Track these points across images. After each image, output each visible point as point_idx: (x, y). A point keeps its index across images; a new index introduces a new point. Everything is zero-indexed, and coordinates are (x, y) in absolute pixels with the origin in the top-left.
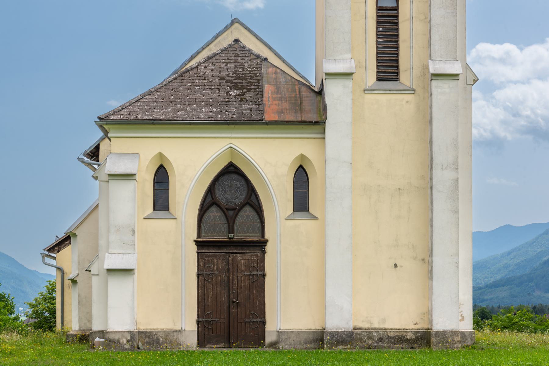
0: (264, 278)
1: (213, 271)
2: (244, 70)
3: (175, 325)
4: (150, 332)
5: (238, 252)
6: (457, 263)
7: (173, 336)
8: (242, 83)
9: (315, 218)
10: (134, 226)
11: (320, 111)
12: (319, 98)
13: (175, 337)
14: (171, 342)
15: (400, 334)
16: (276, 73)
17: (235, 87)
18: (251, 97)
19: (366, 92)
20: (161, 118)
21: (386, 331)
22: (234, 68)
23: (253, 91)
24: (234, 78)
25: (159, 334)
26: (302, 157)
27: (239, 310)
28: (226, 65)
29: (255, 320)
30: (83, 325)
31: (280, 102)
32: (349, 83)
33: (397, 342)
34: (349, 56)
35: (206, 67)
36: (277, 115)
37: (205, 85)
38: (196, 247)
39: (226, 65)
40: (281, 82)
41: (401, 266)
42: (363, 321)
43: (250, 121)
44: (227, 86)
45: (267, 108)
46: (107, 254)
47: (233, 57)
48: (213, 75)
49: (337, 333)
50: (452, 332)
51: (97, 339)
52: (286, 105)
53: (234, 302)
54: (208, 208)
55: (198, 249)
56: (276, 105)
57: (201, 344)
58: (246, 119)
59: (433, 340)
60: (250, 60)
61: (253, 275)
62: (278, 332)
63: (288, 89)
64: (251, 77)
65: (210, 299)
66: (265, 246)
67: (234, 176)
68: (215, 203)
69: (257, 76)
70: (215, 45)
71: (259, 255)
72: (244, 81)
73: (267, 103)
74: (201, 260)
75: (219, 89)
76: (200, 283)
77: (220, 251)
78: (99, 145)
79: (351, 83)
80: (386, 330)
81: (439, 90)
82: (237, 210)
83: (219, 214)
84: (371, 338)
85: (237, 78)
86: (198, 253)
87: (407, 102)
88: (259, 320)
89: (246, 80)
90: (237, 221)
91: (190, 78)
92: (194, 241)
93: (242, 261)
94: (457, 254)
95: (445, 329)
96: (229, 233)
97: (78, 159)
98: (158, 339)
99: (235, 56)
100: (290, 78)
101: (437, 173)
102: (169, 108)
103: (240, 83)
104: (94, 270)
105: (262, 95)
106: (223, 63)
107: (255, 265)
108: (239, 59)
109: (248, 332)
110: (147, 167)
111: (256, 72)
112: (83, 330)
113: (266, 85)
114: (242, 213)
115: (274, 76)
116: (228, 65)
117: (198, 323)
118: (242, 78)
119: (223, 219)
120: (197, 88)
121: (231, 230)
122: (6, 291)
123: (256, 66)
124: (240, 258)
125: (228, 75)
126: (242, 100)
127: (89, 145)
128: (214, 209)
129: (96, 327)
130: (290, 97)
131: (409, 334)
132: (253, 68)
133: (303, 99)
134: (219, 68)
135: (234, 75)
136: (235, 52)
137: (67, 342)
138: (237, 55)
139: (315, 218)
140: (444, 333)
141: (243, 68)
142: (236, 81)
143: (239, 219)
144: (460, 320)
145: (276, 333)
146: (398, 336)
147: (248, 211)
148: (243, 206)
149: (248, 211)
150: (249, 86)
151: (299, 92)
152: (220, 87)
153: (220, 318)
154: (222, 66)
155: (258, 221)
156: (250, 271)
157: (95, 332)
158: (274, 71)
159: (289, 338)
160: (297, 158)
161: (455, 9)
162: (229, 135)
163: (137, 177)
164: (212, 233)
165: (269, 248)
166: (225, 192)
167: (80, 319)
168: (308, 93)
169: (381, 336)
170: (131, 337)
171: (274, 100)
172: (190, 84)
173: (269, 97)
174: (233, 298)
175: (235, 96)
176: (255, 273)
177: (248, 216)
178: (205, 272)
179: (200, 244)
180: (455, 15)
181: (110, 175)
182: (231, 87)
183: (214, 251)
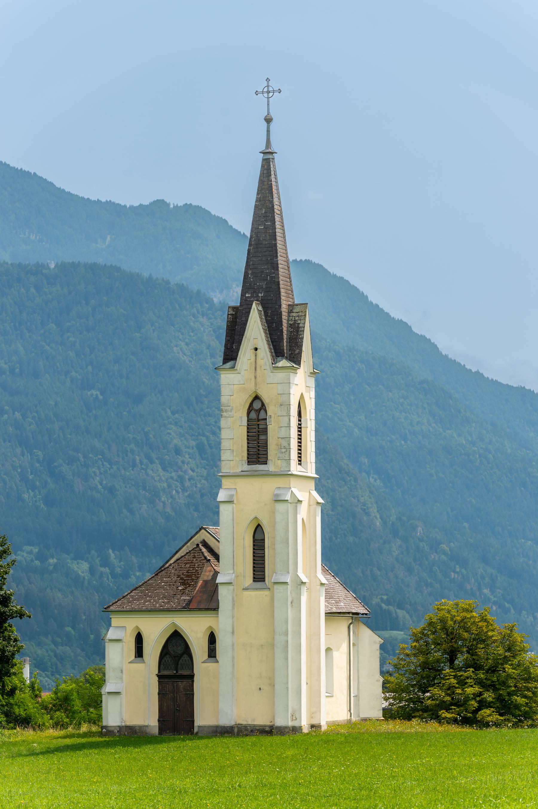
3: (145, 722)
4: (132, 726)
5: (179, 681)
6: (287, 688)
7: (144, 729)
10: (122, 667)
13: (145, 729)
14: (142, 732)
17: (183, 584)
19: (244, 590)
24: (186, 576)
25: (136, 727)
29: (189, 719)
32: (231, 587)
38: (157, 678)
41: (263, 689)
42: (243, 721)
49: (224, 727)
55: (159, 679)
57: (160, 733)
61: (187, 694)
62: (198, 726)
65: (165, 708)
71: (190, 682)
72: (190, 579)
80: (255, 726)
81: (278, 591)
84: (247, 730)
87: (266, 595)
90: (180, 663)
92: (156, 675)
93: (182, 686)
94: (287, 683)
95: (281, 725)
98: (136, 730)
107: (189, 688)
109: (185, 726)
110: (130, 634)
114: (182, 658)
117: (159, 721)
124: (180, 684)
131: (267, 728)
134: (181, 568)
140: (280, 727)
144: (295, 720)
147: (185, 657)
149: (185, 657)
155: (191, 663)
156: (186, 692)
162: (172, 616)
164: (167, 670)
169: (252, 729)
170: (119, 729)
172: (160, 581)
176: (188, 693)
179: (160, 677)
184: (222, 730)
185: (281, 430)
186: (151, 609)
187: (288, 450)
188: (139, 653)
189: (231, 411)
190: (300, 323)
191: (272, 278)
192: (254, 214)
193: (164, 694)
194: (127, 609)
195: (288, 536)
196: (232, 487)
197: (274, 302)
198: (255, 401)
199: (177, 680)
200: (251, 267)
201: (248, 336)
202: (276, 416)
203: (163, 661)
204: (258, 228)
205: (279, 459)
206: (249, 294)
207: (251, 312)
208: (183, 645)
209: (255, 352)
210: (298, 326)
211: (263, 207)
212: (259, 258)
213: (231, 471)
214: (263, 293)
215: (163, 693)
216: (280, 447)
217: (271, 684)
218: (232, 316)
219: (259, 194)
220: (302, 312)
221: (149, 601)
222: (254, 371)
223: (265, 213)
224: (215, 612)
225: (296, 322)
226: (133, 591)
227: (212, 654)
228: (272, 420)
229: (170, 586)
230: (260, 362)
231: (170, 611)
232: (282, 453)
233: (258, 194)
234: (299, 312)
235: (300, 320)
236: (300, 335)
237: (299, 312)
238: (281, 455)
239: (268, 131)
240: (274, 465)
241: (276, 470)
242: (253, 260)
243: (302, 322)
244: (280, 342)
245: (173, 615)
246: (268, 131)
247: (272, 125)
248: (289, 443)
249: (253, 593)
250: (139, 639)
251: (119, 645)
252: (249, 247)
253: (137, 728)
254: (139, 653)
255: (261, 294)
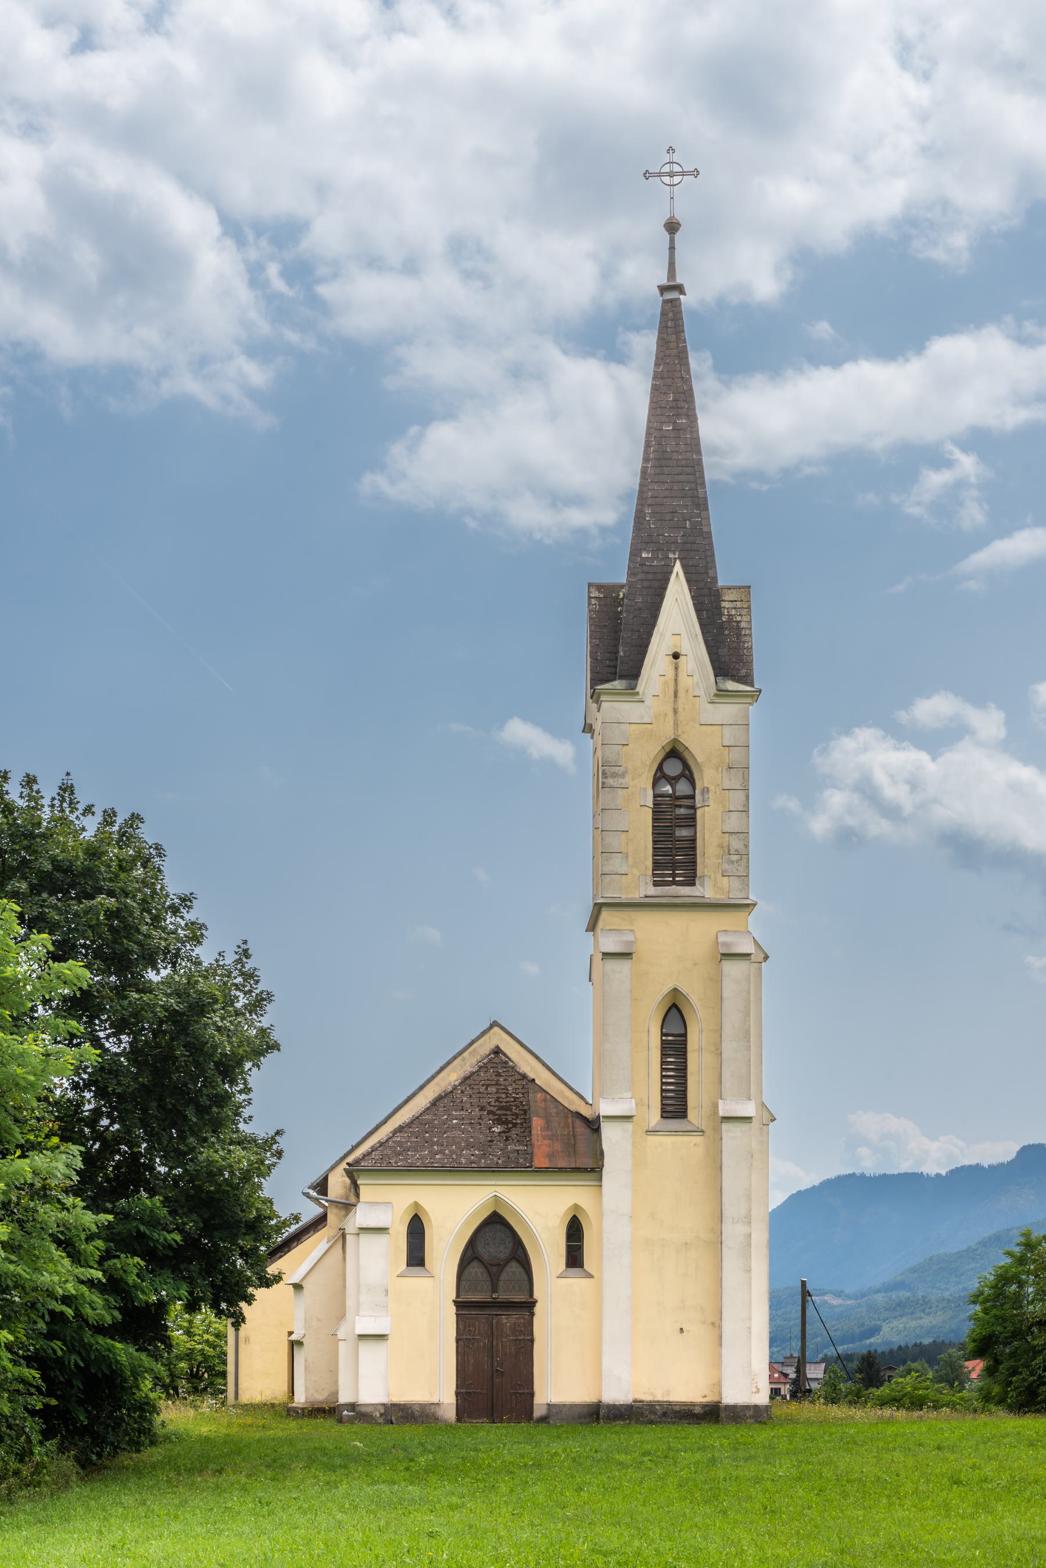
0: (533, 1344)
1: (474, 1335)
2: (507, 1097)
4: (405, 1405)
5: (502, 1313)
6: (749, 1328)
8: (506, 1115)
9: (591, 1276)
11: (596, 1154)
12: (595, 1136)
13: (432, 1410)
15: (687, 1408)
16: (545, 1100)
17: (499, 1121)
18: (517, 1135)
19: (648, 1133)
20: (418, 1164)
21: (671, 1405)
22: (496, 1093)
23: (519, 1126)
26: (576, 1207)
27: (504, 1379)
28: (487, 1089)
30: (310, 1396)
31: (551, 1142)
32: (628, 1126)
33: (683, 1416)
34: (629, 1095)
35: (462, 1092)
36: (547, 1160)
37: (463, 1118)
38: (454, 1308)
39: (487, 1089)
40: (551, 1114)
41: (688, 1331)
42: (645, 1393)
43: (517, 1167)
44: (490, 1120)
45: (536, 1150)
46: (357, 1317)
47: (493, 1077)
48: (471, 1103)
50: (744, 1406)
51: (345, 1413)
52: (558, 1146)
53: (498, 1371)
54: (469, 1263)
55: (457, 1310)
56: (546, 1145)
57: (459, 1418)
58: (513, 1166)
59: (722, 1415)
60: (515, 1082)
61: (520, 1340)
62: (549, 1405)
63: (559, 1124)
64: (517, 1107)
66: (534, 1306)
67: (499, 1227)
68: (477, 1258)
69: (524, 1105)
70: (470, 1054)
71: (526, 1317)
72: (509, 1113)
73: (536, 1143)
74: (460, 1323)
75: (480, 1124)
76: (460, 1349)
77: (482, 1313)
78: (327, 1175)
79: (631, 1126)
80: (670, 1404)
82: (501, 1266)
83: (481, 1270)
85: (501, 1108)
86: (457, 1314)
87: (695, 1145)
88: (527, 1391)
89: (511, 1110)
90: (502, 1278)
91: (444, 1107)
92: (453, 1301)
93: (508, 1324)
94: (750, 1319)
95: (736, 1402)
96: (493, 1292)
97: (304, 1194)
99: (496, 1075)
100: (561, 1108)
101: (728, 1228)
102: (425, 1151)
103: (504, 1115)
104: (341, 1335)
105: (530, 1132)
106: (483, 1085)
107: (523, 1329)
108: (502, 1079)
110: (401, 1218)
111: (521, 1100)
112: (310, 1402)
113: (535, 1118)
114: (507, 1269)
115: (543, 1105)
116: (489, 1089)
117: (457, 1394)
118: (508, 1108)
119: (486, 1275)
120: (455, 1121)
121: (494, 1290)
122: (1032, 1424)
123: (522, 1091)
124: (505, 1321)
125: (489, 1103)
126: (507, 1139)
127: (315, 1176)
128: (475, 1264)
129: (344, 1398)
130: (562, 1135)
131: (697, 1408)
132: (517, 1094)
133: (578, 1137)
135: (497, 1104)
136: (496, 1070)
137: (288, 1415)
138: (499, 1075)
139: (591, 1276)
141: (507, 1093)
142: (499, 1112)
143: (504, 1276)
144: (755, 1393)
145: (547, 1407)
146: (684, 1410)
148: (508, 1261)
149: (514, 1267)
150: (514, 1119)
151: (573, 1127)
152: (481, 1121)
153: (482, 1389)
154: (481, 1090)
155: (526, 1278)
156: (516, 1336)
157: (342, 1405)
158: (543, 1098)
159: (561, 1412)
160: (570, 1208)
161: (749, 1041)
163: (390, 1231)
165: (537, 1309)
166: (488, 1244)
167: (307, 1390)
168: (583, 1129)
169: (665, 1410)
171: (544, 1139)
172: (445, 1117)
173: (538, 1135)
174: (497, 1366)
175: (500, 1133)
177: (514, 1273)
178: (465, 1337)
179: (459, 1305)
180: (749, 1049)
181: (361, 1229)
182: (493, 1121)
183: (475, 1313)
184: (609, 1412)
185: (729, 818)
186: (451, 1167)
187: (744, 856)
188: (416, 1257)
189: (623, 775)
190: (740, 621)
191: (694, 525)
192: (651, 402)
193: (469, 1339)
194: (399, 1166)
195: (749, 1026)
196: (623, 928)
197: (703, 571)
198: (668, 760)
199: (498, 1313)
200: (649, 501)
201: (661, 630)
202: (718, 790)
203: (466, 1273)
204: (661, 430)
205: (724, 874)
206: (648, 553)
207: (671, 580)
208: (509, 1243)
209: (674, 660)
210: (738, 626)
211: (669, 390)
212: (666, 486)
213: (623, 896)
214: (677, 553)
215: (466, 1339)
216: (726, 851)
217: (705, 1321)
218: (599, 602)
219: (660, 365)
220: (741, 601)
221: (441, 1152)
222: (673, 698)
223: (673, 400)
224: (592, 1175)
225: (732, 619)
226: (396, 1133)
227: (575, 1258)
228: (711, 797)
229: (474, 1126)
230: (684, 681)
231: (493, 1171)
232: (732, 862)
233: (657, 365)
234: (736, 601)
235: (740, 615)
236: (744, 642)
237: (736, 601)
238: (726, 866)
239: (672, 248)
240: (715, 885)
241: (719, 897)
242: (654, 489)
243: (745, 619)
244: (718, 648)
245: (497, 1180)
246: (672, 248)
247: (677, 236)
248: (745, 843)
249: (668, 1140)
250: (416, 1229)
251: (381, 1240)
252: (643, 463)
253: (416, 1408)
254: (416, 1257)
255: (675, 554)
